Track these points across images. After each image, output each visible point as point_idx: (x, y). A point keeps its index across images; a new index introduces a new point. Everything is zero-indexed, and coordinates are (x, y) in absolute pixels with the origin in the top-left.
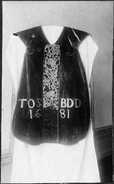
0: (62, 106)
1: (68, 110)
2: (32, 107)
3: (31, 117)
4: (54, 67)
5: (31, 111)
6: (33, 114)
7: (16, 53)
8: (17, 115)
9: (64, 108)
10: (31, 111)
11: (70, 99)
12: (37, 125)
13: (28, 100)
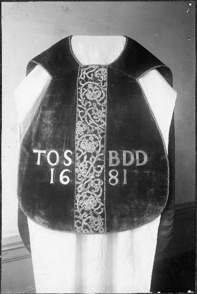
0: (111, 164)
1: (125, 171)
2: (55, 164)
3: (52, 182)
4: (83, 139)
5: (52, 170)
6: (56, 177)
7: (28, 89)
8: (21, 183)
9: (112, 168)
10: (52, 170)
11: (128, 151)
12: (48, 200)
13: (47, 152)
